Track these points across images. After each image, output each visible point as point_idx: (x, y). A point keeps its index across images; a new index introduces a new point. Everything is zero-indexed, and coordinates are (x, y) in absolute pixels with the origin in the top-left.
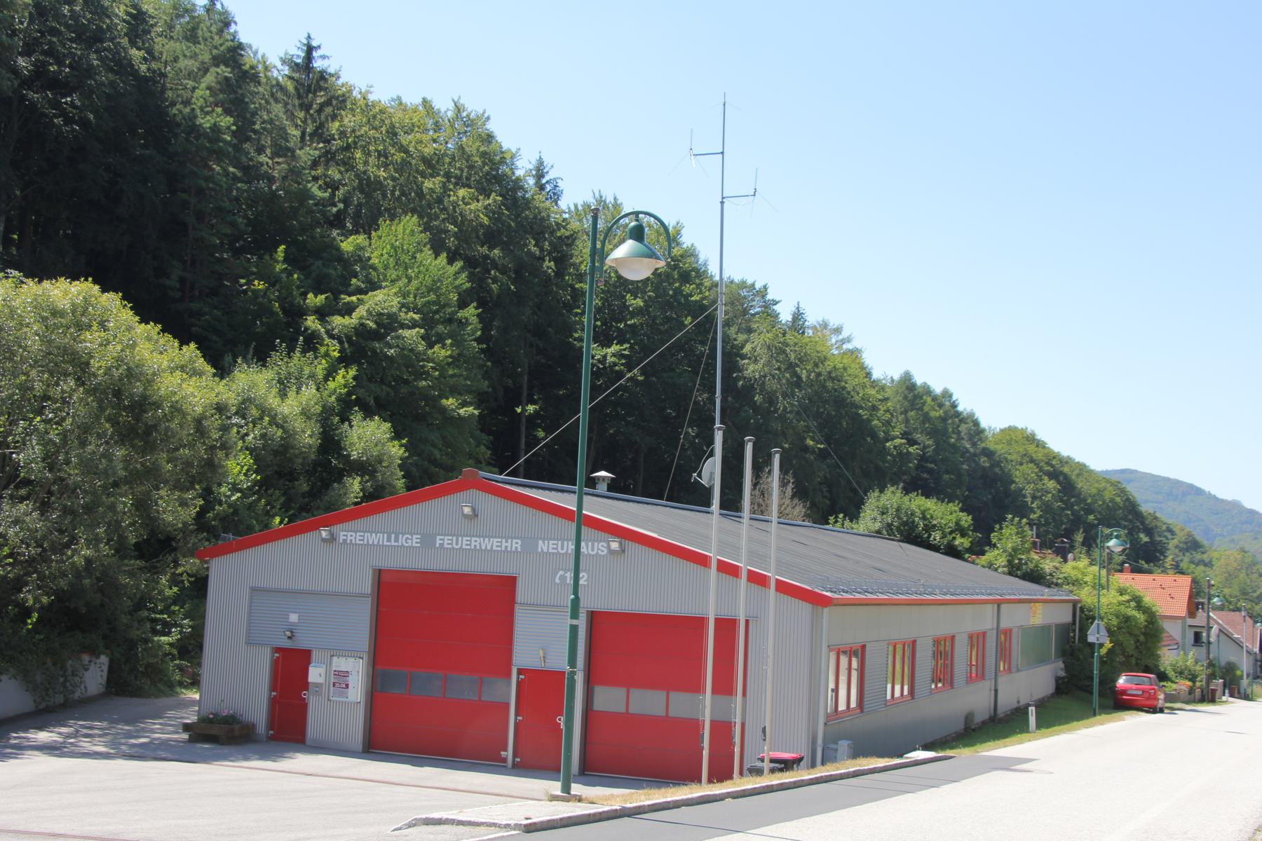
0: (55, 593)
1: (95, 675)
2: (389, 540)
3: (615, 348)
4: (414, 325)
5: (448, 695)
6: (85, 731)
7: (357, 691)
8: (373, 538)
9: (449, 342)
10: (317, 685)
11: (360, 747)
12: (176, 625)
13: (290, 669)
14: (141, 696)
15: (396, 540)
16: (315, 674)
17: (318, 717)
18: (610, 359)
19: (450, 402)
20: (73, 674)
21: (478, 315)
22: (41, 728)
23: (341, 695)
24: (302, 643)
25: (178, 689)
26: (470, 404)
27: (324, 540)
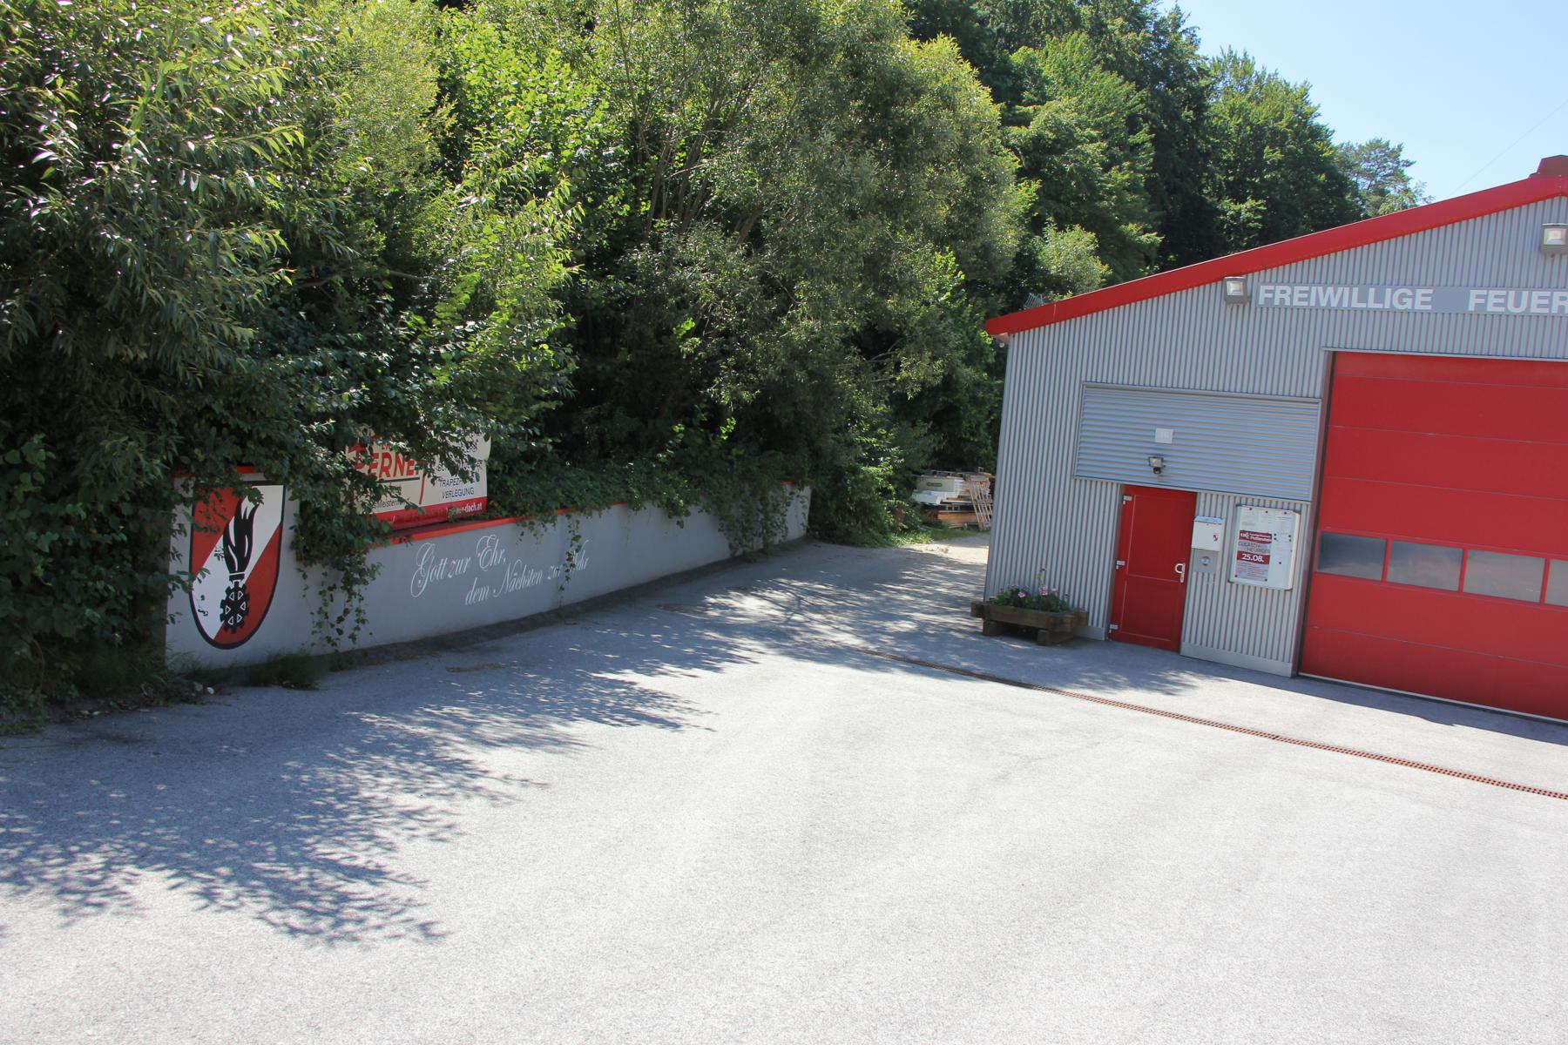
0: (760, 385)
1: (795, 515)
2: (1363, 298)
3: (1250, 203)
4: (1092, 140)
5: (1390, 578)
6: (809, 600)
7: (1285, 569)
8: (1328, 296)
9: (1126, 164)
10: (1207, 555)
11: (1287, 667)
12: (885, 454)
13: (1156, 525)
14: (843, 543)
15: (1379, 298)
16: (1204, 535)
17: (1205, 607)
18: (1244, 215)
19: (1132, 228)
20: (775, 510)
21: (1152, 140)
22: (745, 589)
23: (1252, 576)
24: (1176, 480)
25: (893, 537)
26: (1151, 231)
27: (1230, 300)
